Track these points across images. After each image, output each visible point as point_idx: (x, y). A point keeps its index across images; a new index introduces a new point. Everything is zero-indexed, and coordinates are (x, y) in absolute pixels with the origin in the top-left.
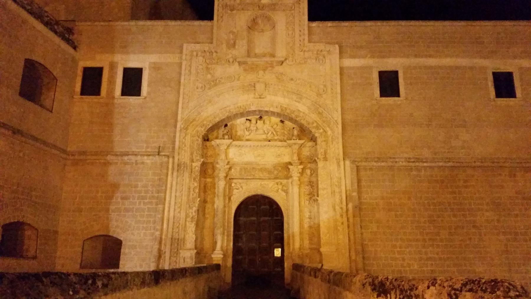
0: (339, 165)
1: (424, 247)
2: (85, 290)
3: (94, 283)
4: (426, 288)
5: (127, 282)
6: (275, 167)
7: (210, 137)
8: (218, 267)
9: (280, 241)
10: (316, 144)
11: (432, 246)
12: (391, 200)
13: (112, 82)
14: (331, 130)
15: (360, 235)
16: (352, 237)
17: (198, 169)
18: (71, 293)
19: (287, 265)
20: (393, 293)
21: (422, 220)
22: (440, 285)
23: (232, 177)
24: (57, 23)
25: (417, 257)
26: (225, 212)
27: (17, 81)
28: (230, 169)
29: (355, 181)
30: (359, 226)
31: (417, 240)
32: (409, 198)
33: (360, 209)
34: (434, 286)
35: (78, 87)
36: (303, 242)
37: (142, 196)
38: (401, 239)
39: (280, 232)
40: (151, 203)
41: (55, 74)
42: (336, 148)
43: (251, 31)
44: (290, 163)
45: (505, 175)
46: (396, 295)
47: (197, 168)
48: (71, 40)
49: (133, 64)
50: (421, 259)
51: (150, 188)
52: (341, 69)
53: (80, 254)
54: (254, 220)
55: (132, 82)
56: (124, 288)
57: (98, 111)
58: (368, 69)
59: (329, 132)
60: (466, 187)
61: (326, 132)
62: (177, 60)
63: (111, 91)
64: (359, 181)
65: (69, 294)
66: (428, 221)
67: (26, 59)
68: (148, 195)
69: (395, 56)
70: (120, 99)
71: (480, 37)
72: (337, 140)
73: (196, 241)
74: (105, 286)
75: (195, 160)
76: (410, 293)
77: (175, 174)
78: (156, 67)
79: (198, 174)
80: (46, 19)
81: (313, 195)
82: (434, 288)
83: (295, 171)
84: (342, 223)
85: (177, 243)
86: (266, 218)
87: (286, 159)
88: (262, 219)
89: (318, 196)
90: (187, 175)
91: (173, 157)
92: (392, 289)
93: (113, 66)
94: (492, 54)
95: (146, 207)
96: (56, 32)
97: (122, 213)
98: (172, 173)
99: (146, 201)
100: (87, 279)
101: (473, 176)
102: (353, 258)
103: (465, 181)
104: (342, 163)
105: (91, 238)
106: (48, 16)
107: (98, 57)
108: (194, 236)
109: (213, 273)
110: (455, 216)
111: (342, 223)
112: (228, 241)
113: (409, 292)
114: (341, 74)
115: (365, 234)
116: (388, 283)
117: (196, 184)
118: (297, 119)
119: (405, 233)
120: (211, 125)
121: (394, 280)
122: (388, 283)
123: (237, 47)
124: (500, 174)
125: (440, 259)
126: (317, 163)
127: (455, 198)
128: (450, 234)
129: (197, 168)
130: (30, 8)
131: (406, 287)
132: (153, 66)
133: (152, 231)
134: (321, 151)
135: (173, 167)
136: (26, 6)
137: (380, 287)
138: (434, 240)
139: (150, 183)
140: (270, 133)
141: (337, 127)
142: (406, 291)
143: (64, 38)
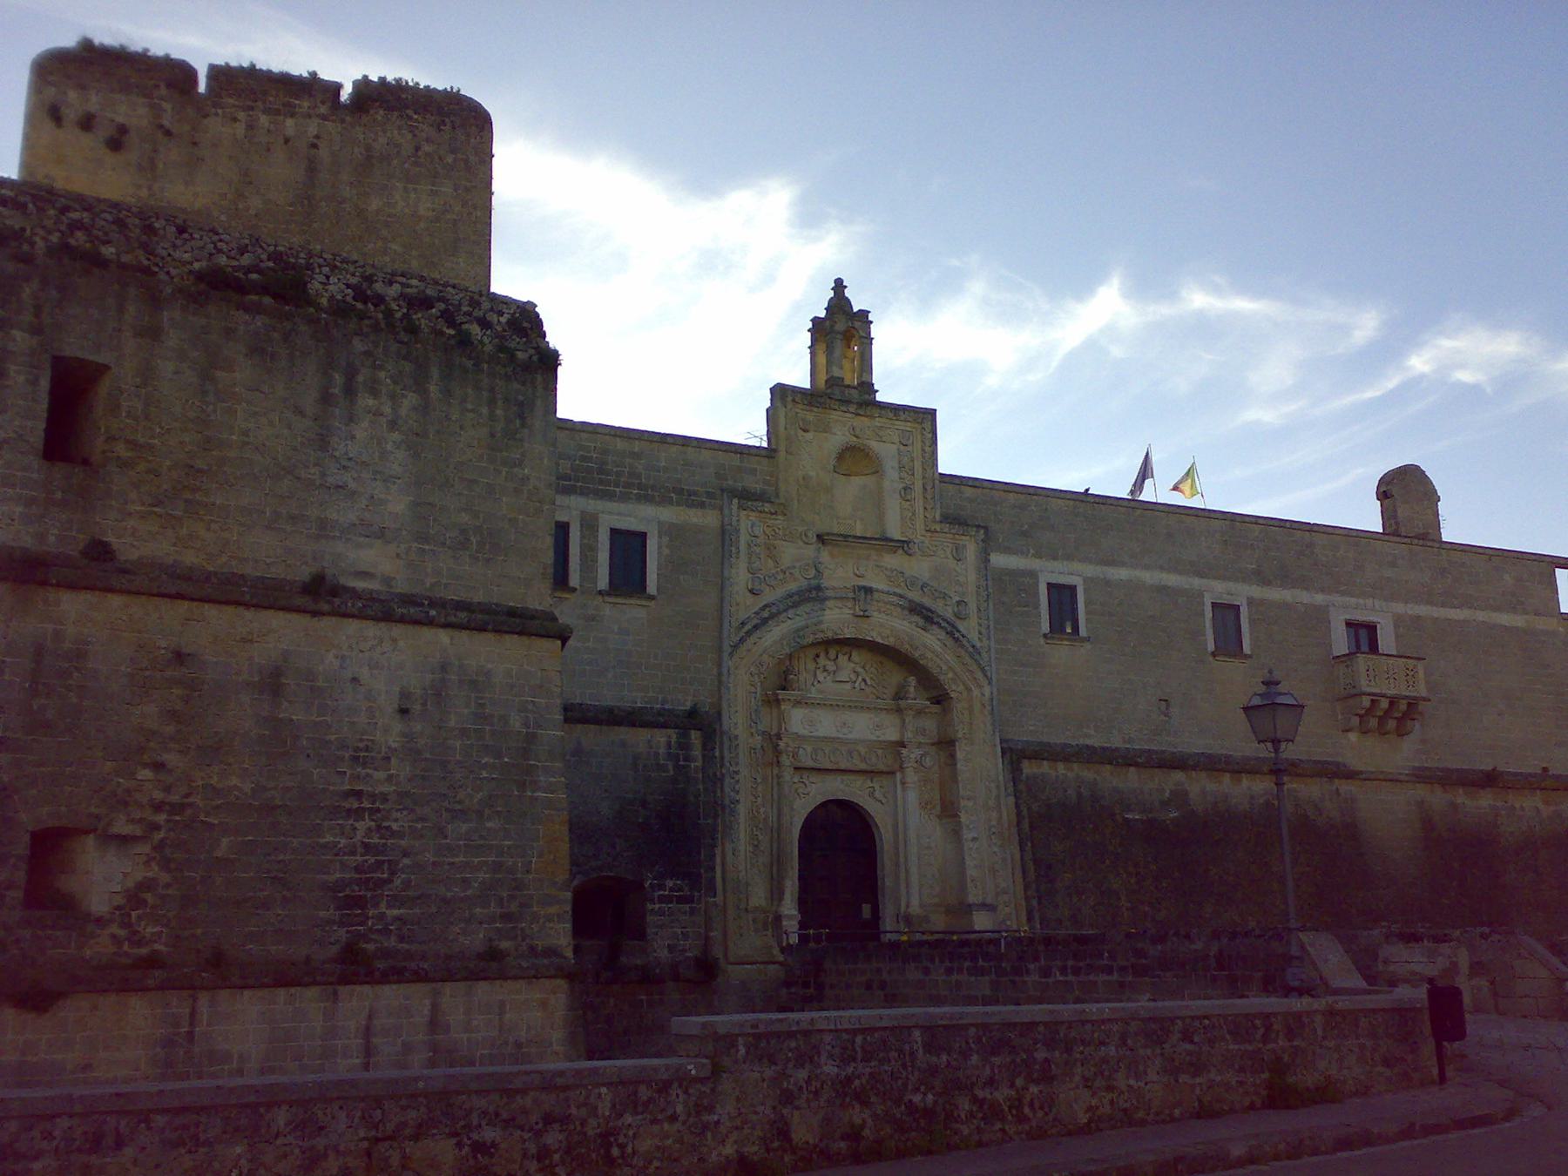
67: (932, 413)
78: (673, 532)
81: (948, 810)
83: (911, 755)
87: (892, 735)
93: (589, 523)
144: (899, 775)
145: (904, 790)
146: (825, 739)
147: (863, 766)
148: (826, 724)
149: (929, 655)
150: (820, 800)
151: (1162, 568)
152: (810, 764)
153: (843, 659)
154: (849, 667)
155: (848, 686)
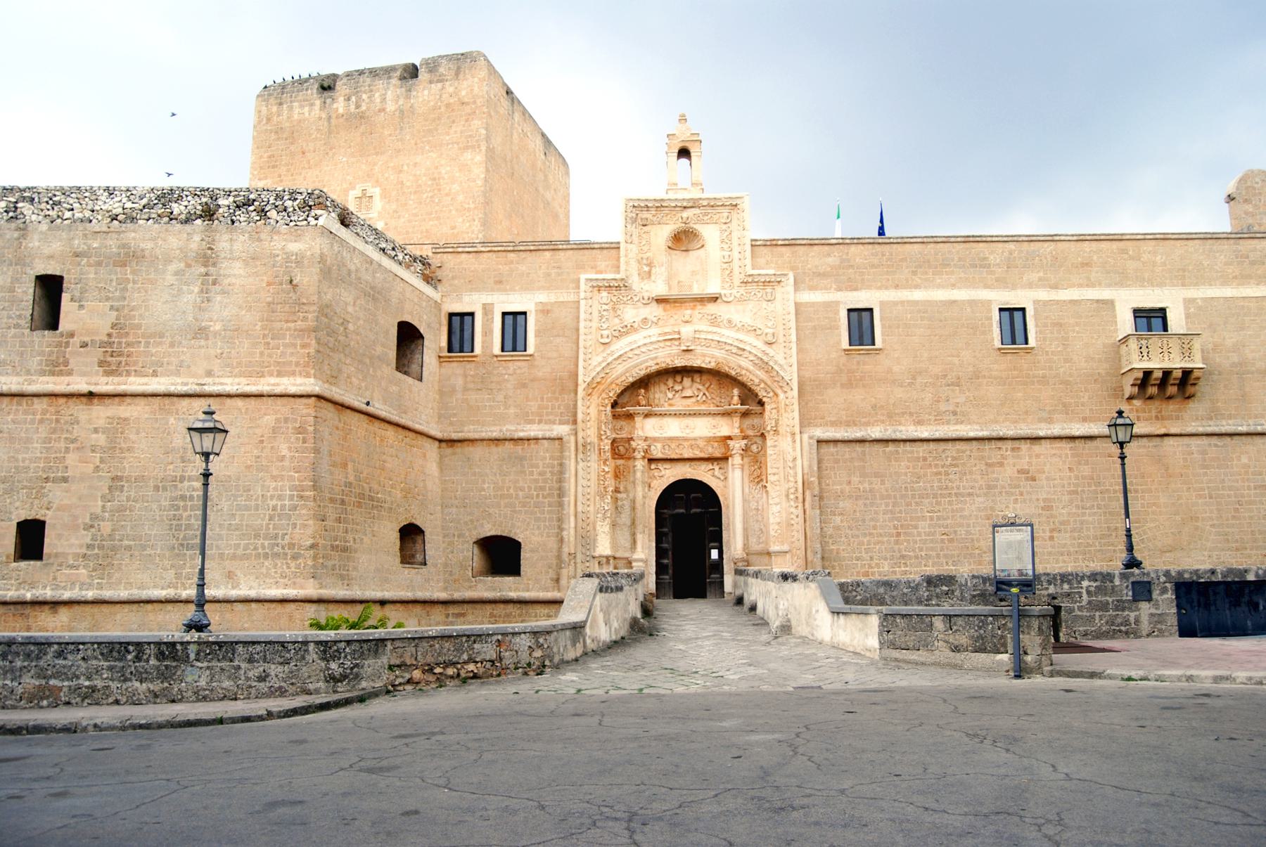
6: (710, 440)
7: (620, 401)
9: (717, 539)
13: (487, 332)
17: (608, 447)
29: (815, 462)
44: (730, 438)
50: (892, 558)
51: (548, 475)
52: (798, 306)
58: (831, 306)
59: (782, 396)
60: (955, 466)
63: (487, 345)
64: (820, 462)
71: (985, 259)
77: (580, 456)
78: (545, 310)
88: (693, 511)
90: (594, 456)
93: (488, 309)
94: (1002, 283)
101: (964, 452)
104: (798, 437)
114: (797, 313)
123: (653, 278)
132: (540, 308)
135: (577, 450)
146: (671, 439)
148: (672, 428)
150: (672, 480)
152: (660, 456)
155: (693, 400)
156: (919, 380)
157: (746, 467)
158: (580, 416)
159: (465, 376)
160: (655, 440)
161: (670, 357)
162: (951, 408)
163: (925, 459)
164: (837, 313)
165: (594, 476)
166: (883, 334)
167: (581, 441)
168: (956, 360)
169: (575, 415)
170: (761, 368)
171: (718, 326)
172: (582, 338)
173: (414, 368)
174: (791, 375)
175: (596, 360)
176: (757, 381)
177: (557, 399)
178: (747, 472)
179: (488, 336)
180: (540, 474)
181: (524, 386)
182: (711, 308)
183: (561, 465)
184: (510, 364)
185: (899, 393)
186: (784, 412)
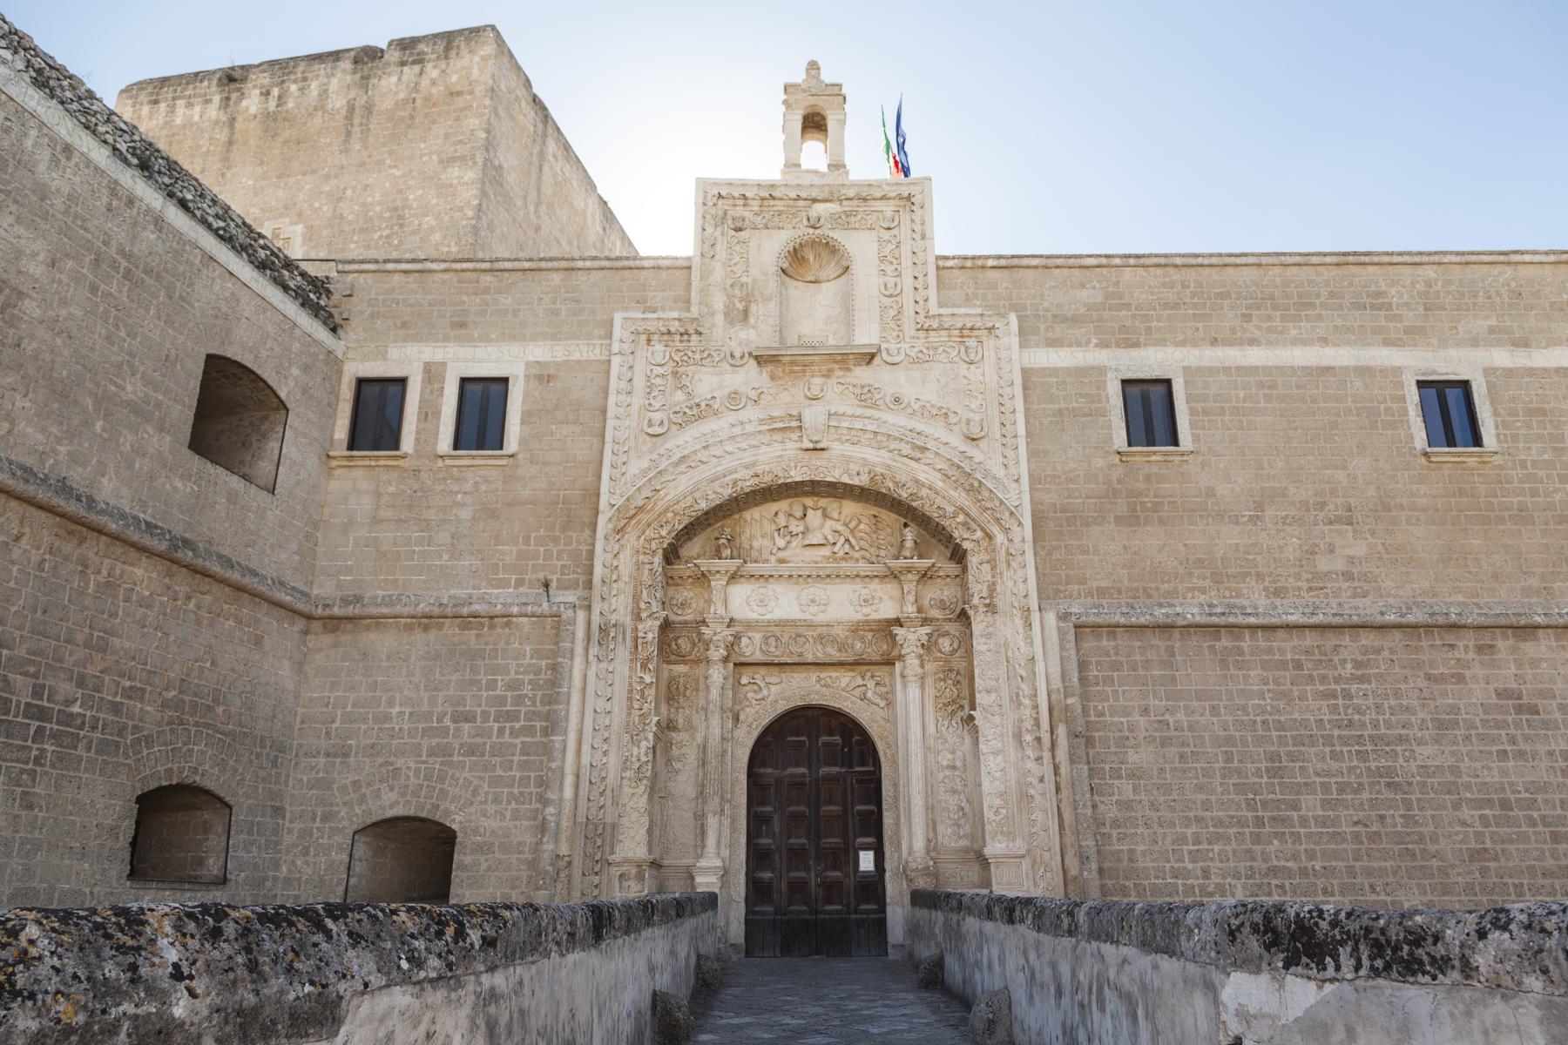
0: (1028, 625)
1: (1257, 839)
2: (439, 956)
3: (460, 934)
4: (1474, 936)
5: (540, 935)
6: (856, 628)
8: (711, 901)
9: (873, 828)
10: (965, 569)
11: (1281, 836)
12: (1167, 717)
13: (429, 413)
14: (1006, 530)
15: (1089, 811)
16: (1068, 816)
18: (405, 965)
19: (894, 889)
20: (1344, 953)
21: (1251, 767)
22: (1529, 927)
23: (742, 659)
24: (289, 264)
25: (1242, 866)
26: (724, 752)
27: (183, 413)
28: (737, 637)
30: (1087, 789)
31: (1241, 823)
32: (1215, 711)
33: (1089, 742)
34: (1505, 928)
35: (341, 432)
36: (935, 831)
37: (507, 712)
38: (1199, 820)
39: (873, 807)
40: (529, 731)
41: (283, 395)
42: (1020, 580)
43: (788, 280)
44: (898, 622)
45: (1466, 647)
46: (1359, 960)
47: (650, 635)
48: (323, 308)
49: (485, 365)
51: (527, 690)
53: (343, 869)
54: (803, 775)
55: (481, 412)
56: (534, 950)
57: (392, 489)
59: (1000, 538)
60: (1363, 679)
61: (991, 538)
62: (596, 354)
63: (426, 436)
64: (1083, 666)
65: (399, 967)
66: (1267, 769)
67: (209, 356)
68: (523, 710)
69: (1161, 342)
70: (451, 457)
71: (1379, 294)
72: (1019, 559)
73: (650, 831)
74: (488, 943)
75: (644, 615)
76: (1411, 954)
77: (594, 650)
78: (543, 376)
79: (653, 649)
80: (262, 254)
81: (961, 703)
82: (1506, 935)
83: (911, 638)
84: (1042, 780)
85: (598, 836)
86: (834, 770)
87: (887, 611)
88: (825, 770)
89: (973, 707)
90: (623, 653)
91: (589, 608)
92: (1342, 943)
93: (433, 374)
94: (1413, 336)
95: (517, 741)
96: (286, 288)
97: (455, 758)
98: (587, 649)
99: (517, 725)
100: (444, 924)
101: (1378, 651)
102: (1074, 872)
103: (1358, 665)
105: (374, 825)
106: (264, 247)
107: (394, 352)
108: (645, 820)
109: (704, 916)
110: (1336, 756)
111: (1042, 780)
112: (733, 830)
113: (1406, 948)
115: (1102, 807)
116: (1324, 925)
117: (648, 679)
118: (914, 504)
119: (1206, 806)
120: (686, 521)
121: (1342, 915)
122: (1324, 925)
123: (752, 320)
124: (1452, 646)
125: (1304, 872)
126: (968, 618)
127: (1334, 709)
128: (1326, 804)
129: (650, 635)
130: (222, 224)
131: (1395, 933)
133: (534, 806)
134: (978, 590)
136: (210, 219)
137: (1293, 937)
138: (1282, 821)
139: (527, 678)
140: (842, 540)
141: (1020, 524)
142: (1397, 949)
143: (305, 303)
144: (898, 665)
145: (905, 686)
146: (781, 624)
147: (843, 657)
148: (785, 603)
149: (924, 492)
150: (782, 707)
151: (1324, 341)
152: (758, 657)
153: (814, 518)
154: (828, 524)
155: (826, 551)
156: (1270, 512)
157: (929, 681)
158: (598, 571)
159: (378, 495)
160: (750, 625)
161: (779, 459)
162: (1341, 566)
163: (1298, 665)
164: (1101, 386)
165: (620, 692)
166: (1193, 425)
167: (596, 619)
168: (1341, 476)
169: (590, 571)
170: (957, 485)
171: (875, 406)
172: (610, 423)
173: (264, 467)
174: (1019, 497)
175: (635, 467)
176: (950, 509)
177: (556, 540)
178: (931, 692)
179: (428, 422)
180: (510, 686)
181: (492, 514)
182: (861, 374)
183: (554, 668)
184: (469, 474)
185: (1230, 537)
186: (1010, 573)
